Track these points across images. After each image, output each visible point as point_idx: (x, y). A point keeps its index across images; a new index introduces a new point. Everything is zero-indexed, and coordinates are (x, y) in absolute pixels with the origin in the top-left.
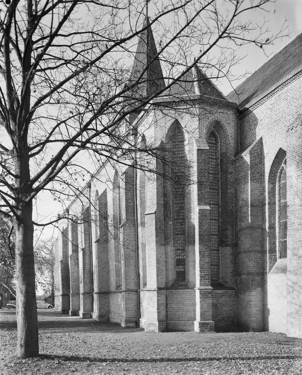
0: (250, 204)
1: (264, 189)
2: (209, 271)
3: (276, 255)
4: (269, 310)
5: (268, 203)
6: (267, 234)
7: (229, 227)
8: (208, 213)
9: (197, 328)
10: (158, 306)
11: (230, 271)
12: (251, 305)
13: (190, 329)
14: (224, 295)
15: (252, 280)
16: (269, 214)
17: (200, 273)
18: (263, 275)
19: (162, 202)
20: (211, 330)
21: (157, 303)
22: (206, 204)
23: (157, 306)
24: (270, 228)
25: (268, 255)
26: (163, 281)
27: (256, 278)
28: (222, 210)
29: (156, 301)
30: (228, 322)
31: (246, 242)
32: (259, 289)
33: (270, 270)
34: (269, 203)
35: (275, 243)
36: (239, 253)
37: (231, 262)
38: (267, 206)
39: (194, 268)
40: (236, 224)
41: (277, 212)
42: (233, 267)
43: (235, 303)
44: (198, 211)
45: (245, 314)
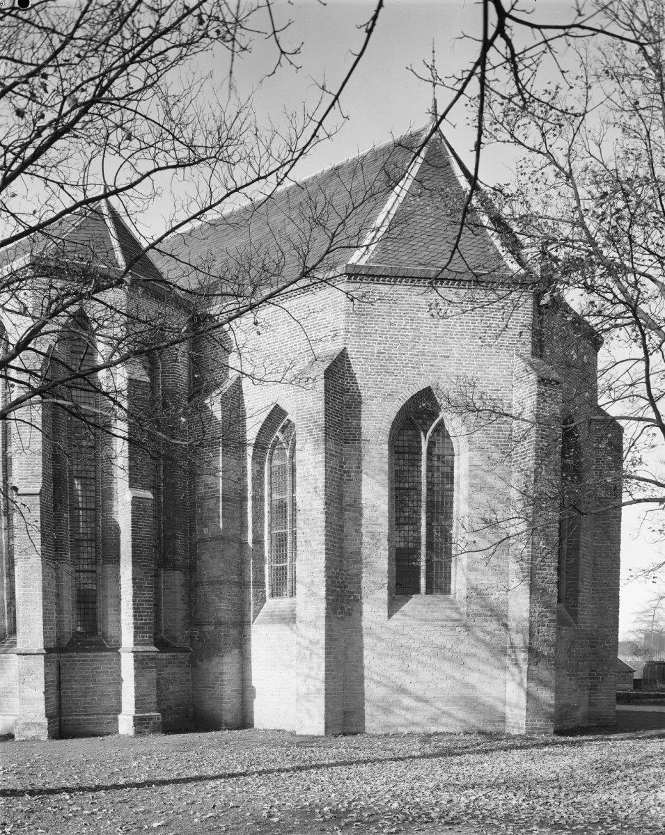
0: (221, 496)
1: (243, 471)
2: (151, 616)
3: (265, 592)
4: (253, 690)
5: (253, 497)
6: (249, 553)
7: (179, 534)
8: (149, 504)
9: (125, 724)
10: (46, 687)
11: (181, 617)
12: (222, 681)
13: (109, 730)
14: (171, 663)
15: (225, 635)
16: (253, 516)
17: (135, 619)
18: (242, 625)
19: (51, 472)
20: (154, 731)
21: (43, 680)
22: (143, 487)
23: (43, 685)
24: (254, 542)
25: (252, 589)
26: (53, 634)
27: (231, 632)
28: (165, 499)
29: (43, 676)
30: (178, 714)
31: (214, 566)
32: (236, 651)
33: (255, 617)
34: (254, 498)
35: (262, 570)
36: (197, 584)
37: (182, 600)
38: (250, 503)
39: (118, 610)
40: (192, 530)
41: (266, 515)
42: (187, 610)
43: (189, 677)
44: (130, 499)
45: (210, 698)
